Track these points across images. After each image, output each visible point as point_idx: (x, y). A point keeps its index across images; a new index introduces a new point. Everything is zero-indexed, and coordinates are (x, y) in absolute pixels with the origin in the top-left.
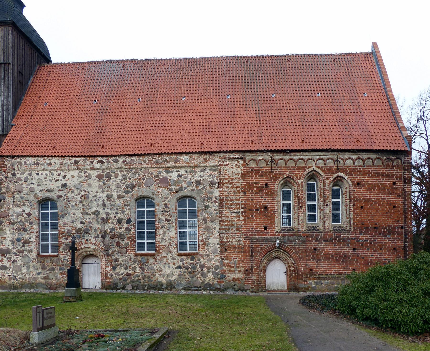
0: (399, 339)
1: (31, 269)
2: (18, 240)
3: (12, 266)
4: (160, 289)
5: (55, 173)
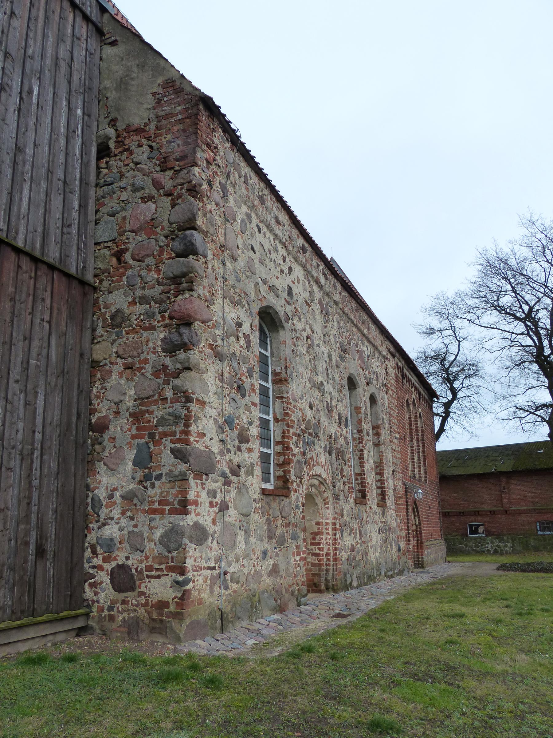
3: (218, 528)
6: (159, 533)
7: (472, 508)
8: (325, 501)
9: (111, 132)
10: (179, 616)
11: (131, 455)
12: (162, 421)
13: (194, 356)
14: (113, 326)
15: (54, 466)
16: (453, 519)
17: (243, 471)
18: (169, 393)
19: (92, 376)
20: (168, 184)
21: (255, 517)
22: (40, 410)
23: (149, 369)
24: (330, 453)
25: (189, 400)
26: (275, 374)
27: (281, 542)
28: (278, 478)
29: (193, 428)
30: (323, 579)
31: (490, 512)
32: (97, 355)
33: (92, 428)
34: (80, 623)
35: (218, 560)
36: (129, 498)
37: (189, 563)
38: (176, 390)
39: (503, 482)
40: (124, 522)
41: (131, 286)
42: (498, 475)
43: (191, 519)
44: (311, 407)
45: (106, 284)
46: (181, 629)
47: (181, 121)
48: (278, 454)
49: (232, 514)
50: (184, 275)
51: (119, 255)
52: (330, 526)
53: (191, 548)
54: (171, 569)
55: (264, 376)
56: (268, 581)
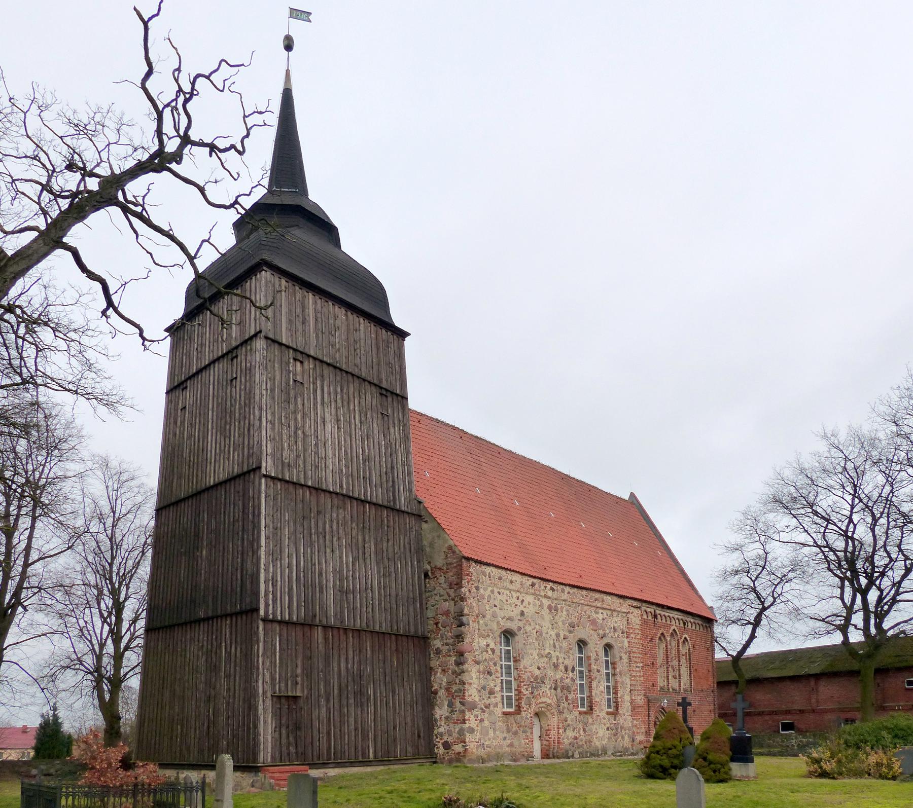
0: (597, 783)
1: (497, 732)
2: (484, 688)
3: (479, 728)
4: (598, 756)
5: (515, 595)
6: (457, 730)
7: (784, 708)
8: (553, 714)
9: (428, 567)
10: (464, 756)
11: (446, 703)
12: (456, 691)
13: (466, 667)
14: (437, 654)
15: (420, 708)
16: (767, 718)
17: (491, 706)
18: (457, 681)
19: (431, 673)
20: (453, 595)
21: (499, 724)
22: (414, 690)
23: (450, 672)
24: (555, 689)
25: (464, 684)
26: (514, 658)
27: (516, 733)
28: (516, 706)
29: (466, 694)
30: (551, 753)
31: (800, 711)
32: (432, 665)
33: (432, 693)
34: (434, 760)
35: (480, 739)
36: (447, 718)
37: (467, 740)
38: (460, 680)
39: (812, 683)
40: (445, 726)
41: (442, 638)
42: (808, 677)
43: (467, 725)
44: (539, 668)
45: (432, 636)
46: (466, 761)
47: (455, 567)
48: (516, 695)
49: (486, 723)
50: (460, 635)
51: (437, 624)
52: (556, 727)
53: (468, 735)
54: (461, 742)
55: (508, 659)
56: (508, 749)
